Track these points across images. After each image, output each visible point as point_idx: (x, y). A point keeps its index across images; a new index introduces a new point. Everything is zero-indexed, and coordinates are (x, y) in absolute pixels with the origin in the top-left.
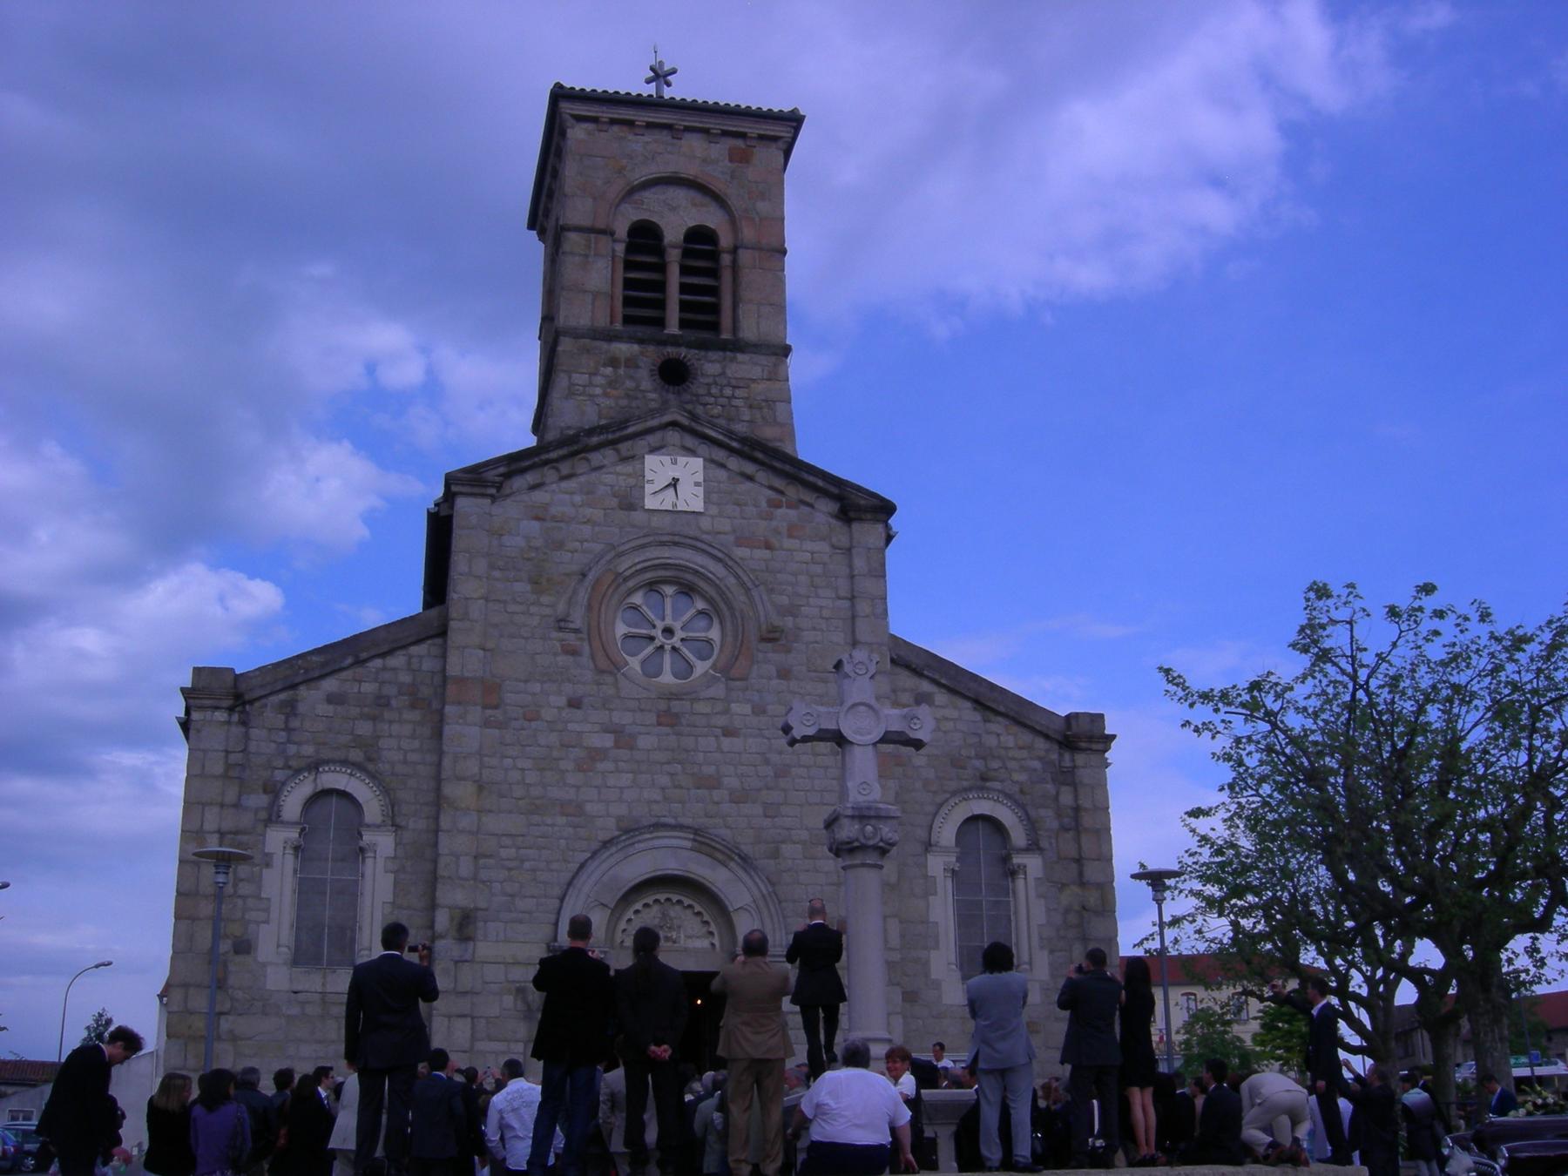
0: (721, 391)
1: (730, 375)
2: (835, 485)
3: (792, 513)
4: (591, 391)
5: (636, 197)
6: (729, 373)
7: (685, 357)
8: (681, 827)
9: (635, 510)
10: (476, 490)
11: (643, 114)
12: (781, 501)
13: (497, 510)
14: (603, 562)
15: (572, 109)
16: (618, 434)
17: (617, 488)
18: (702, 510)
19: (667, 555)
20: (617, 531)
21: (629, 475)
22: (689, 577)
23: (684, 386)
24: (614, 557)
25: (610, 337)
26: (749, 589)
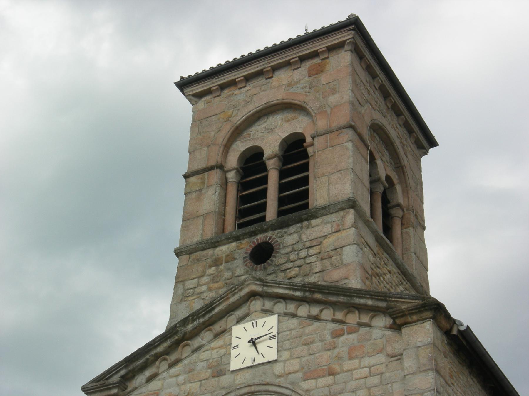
1: (305, 240)
2: (381, 300)
3: (352, 337)
4: (198, 290)
6: (304, 238)
9: (224, 375)
12: (343, 330)
18: (275, 358)
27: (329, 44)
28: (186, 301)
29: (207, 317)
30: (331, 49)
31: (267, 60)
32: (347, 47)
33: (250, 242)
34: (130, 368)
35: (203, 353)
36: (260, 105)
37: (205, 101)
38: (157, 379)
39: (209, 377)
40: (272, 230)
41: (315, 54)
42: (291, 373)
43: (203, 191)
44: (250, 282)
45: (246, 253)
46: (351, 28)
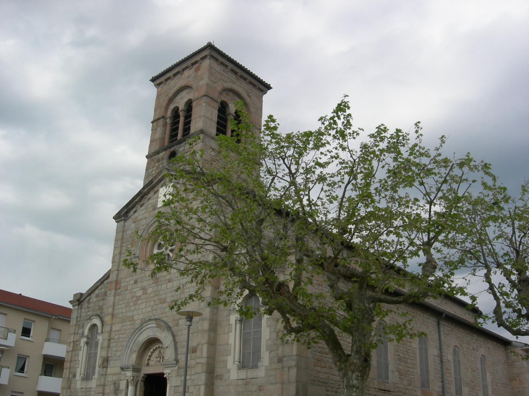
8: (150, 320)
14: (145, 231)
29: (151, 185)
30: (202, 59)
32: (208, 57)
34: (128, 208)
41: (196, 62)
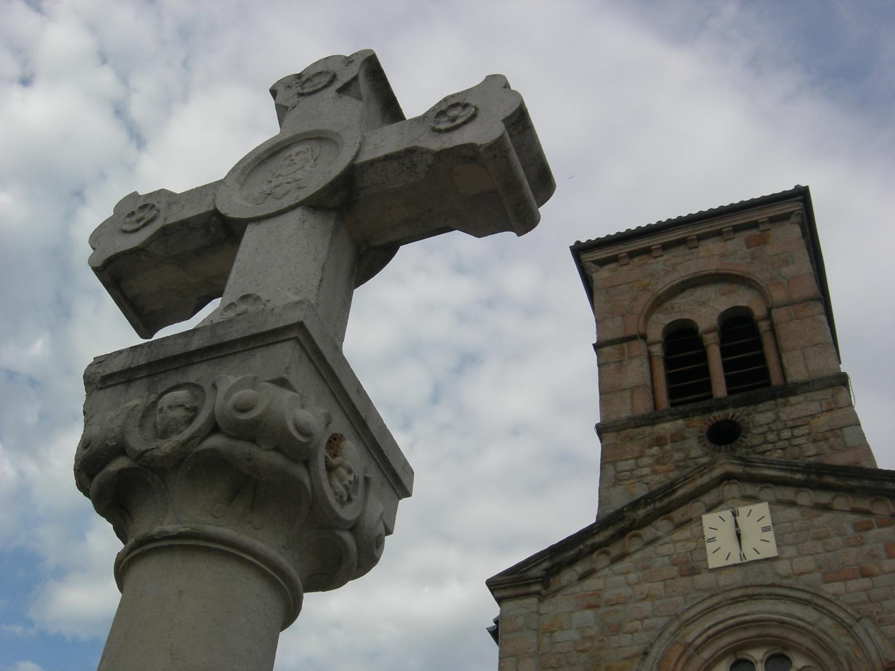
0: (778, 435)
1: (785, 418)
4: (638, 472)
5: (666, 305)
6: (783, 416)
7: (733, 416)
9: (699, 573)
10: (521, 591)
11: (658, 238)
12: (870, 522)
13: (548, 607)
14: (667, 634)
15: (592, 257)
16: (666, 501)
17: (675, 556)
18: (776, 554)
19: (742, 612)
20: (680, 599)
21: (687, 540)
22: (776, 631)
23: (737, 442)
24: (680, 627)
25: (652, 419)
26: (851, 627)
27: (772, 215)
28: (620, 485)
30: (773, 220)
31: (691, 228)
32: (793, 219)
33: (705, 420)
34: (557, 560)
35: (661, 547)
36: (686, 275)
37: (608, 269)
38: (595, 576)
39: (676, 576)
40: (734, 407)
41: (755, 225)
42: (803, 573)
43: (625, 363)
44: (725, 460)
45: (700, 432)
46: (682, 231)
